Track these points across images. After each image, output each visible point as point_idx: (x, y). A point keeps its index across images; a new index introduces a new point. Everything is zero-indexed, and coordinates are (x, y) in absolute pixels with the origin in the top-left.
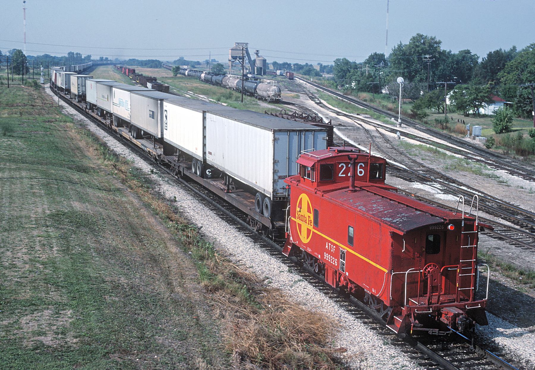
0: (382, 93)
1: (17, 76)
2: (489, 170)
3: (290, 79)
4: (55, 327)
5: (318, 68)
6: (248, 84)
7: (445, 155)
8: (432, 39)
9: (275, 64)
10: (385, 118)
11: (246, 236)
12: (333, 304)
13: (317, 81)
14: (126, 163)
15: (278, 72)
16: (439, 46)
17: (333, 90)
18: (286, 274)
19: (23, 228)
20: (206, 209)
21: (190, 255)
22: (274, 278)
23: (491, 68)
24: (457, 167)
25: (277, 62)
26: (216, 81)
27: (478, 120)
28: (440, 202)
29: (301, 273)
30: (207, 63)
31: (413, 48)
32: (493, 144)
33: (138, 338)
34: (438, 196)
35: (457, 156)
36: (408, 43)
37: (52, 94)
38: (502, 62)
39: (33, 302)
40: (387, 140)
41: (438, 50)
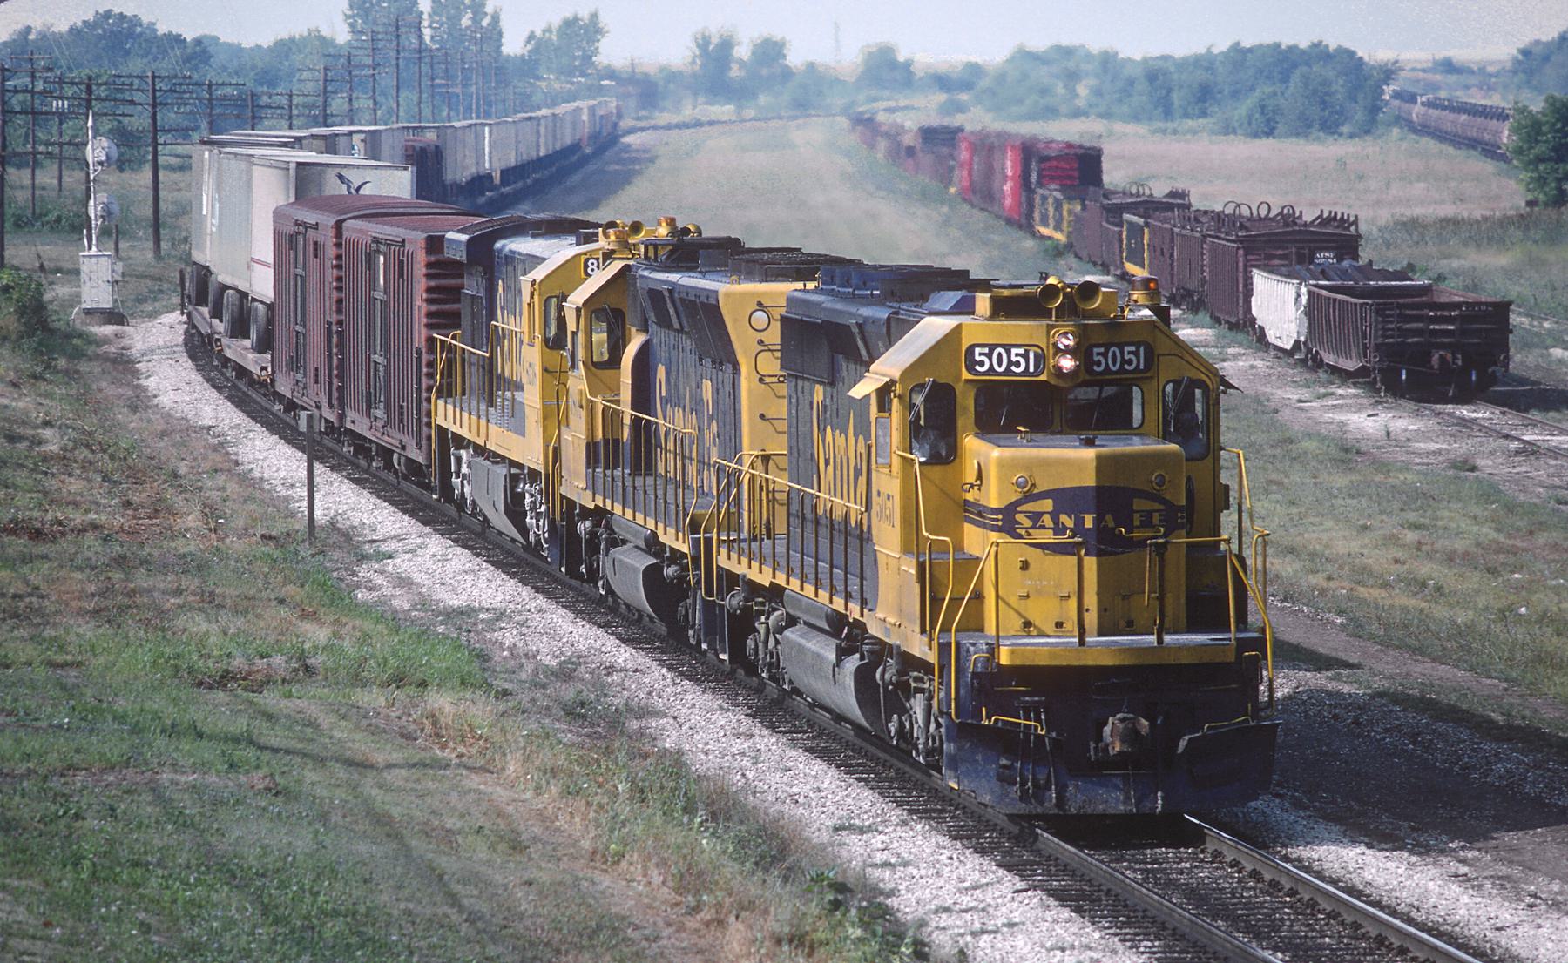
37: (213, 410)
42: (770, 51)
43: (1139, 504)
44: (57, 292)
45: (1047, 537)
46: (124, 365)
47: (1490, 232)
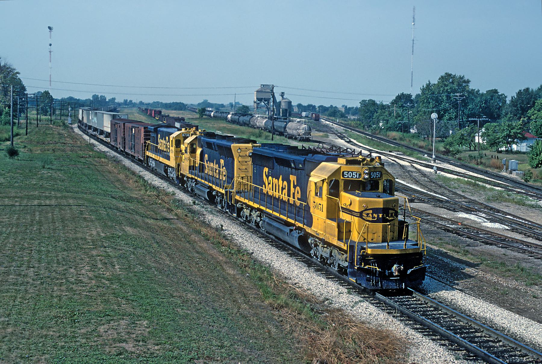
0: (410, 132)
1: (43, 117)
2: (531, 201)
3: (316, 120)
4: (134, 336)
5: (343, 110)
6: (277, 124)
7: (484, 188)
8: (461, 78)
9: (299, 106)
10: (417, 154)
11: (299, 261)
12: (399, 323)
13: (343, 122)
14: (167, 194)
15: (304, 114)
16: (468, 85)
17: (361, 130)
18: (345, 296)
19: (81, 248)
20: (254, 236)
21: (247, 276)
22: (334, 299)
23: (521, 106)
24: (499, 198)
25: (302, 104)
26: (243, 121)
27: (511, 156)
28: (488, 230)
29: (361, 294)
30: (231, 105)
31: (442, 87)
32: (531, 178)
33: (219, 346)
34: (484, 224)
35: (497, 188)
36: (436, 83)
37: (81, 133)
38: (533, 100)
39: (107, 313)
40: (424, 175)
41: (467, 89)
42: (131, 101)
43: (390, 211)
44: (66, 122)
45: (371, 219)
46: (72, 128)
47: (196, 119)
